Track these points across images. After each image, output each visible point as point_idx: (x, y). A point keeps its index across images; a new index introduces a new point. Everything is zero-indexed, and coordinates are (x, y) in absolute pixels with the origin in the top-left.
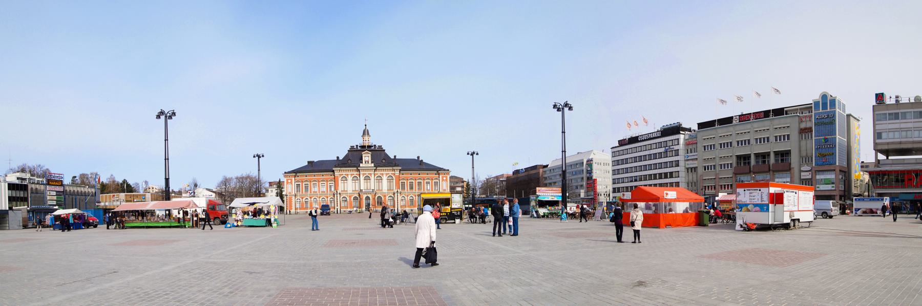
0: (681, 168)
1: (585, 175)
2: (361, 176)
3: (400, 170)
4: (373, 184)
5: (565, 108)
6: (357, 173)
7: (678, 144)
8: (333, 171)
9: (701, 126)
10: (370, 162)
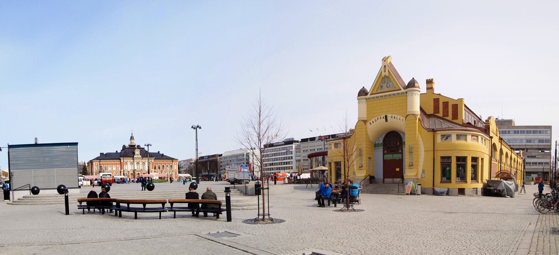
0: (293, 160)
1: (245, 161)
2: (135, 162)
3: (154, 159)
4: (141, 167)
5: (197, 128)
6: (132, 160)
7: (292, 149)
8: (120, 159)
9: (304, 140)
10: (139, 155)
